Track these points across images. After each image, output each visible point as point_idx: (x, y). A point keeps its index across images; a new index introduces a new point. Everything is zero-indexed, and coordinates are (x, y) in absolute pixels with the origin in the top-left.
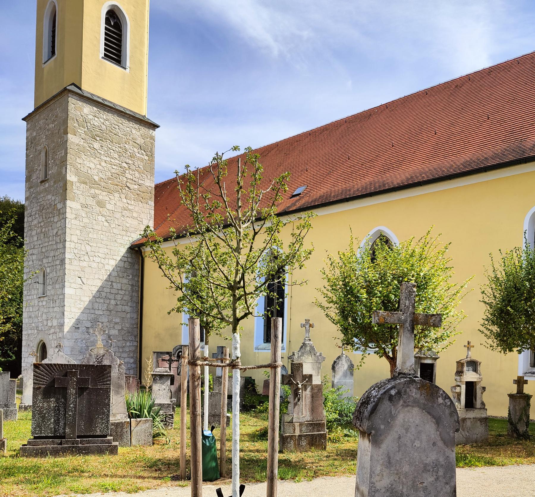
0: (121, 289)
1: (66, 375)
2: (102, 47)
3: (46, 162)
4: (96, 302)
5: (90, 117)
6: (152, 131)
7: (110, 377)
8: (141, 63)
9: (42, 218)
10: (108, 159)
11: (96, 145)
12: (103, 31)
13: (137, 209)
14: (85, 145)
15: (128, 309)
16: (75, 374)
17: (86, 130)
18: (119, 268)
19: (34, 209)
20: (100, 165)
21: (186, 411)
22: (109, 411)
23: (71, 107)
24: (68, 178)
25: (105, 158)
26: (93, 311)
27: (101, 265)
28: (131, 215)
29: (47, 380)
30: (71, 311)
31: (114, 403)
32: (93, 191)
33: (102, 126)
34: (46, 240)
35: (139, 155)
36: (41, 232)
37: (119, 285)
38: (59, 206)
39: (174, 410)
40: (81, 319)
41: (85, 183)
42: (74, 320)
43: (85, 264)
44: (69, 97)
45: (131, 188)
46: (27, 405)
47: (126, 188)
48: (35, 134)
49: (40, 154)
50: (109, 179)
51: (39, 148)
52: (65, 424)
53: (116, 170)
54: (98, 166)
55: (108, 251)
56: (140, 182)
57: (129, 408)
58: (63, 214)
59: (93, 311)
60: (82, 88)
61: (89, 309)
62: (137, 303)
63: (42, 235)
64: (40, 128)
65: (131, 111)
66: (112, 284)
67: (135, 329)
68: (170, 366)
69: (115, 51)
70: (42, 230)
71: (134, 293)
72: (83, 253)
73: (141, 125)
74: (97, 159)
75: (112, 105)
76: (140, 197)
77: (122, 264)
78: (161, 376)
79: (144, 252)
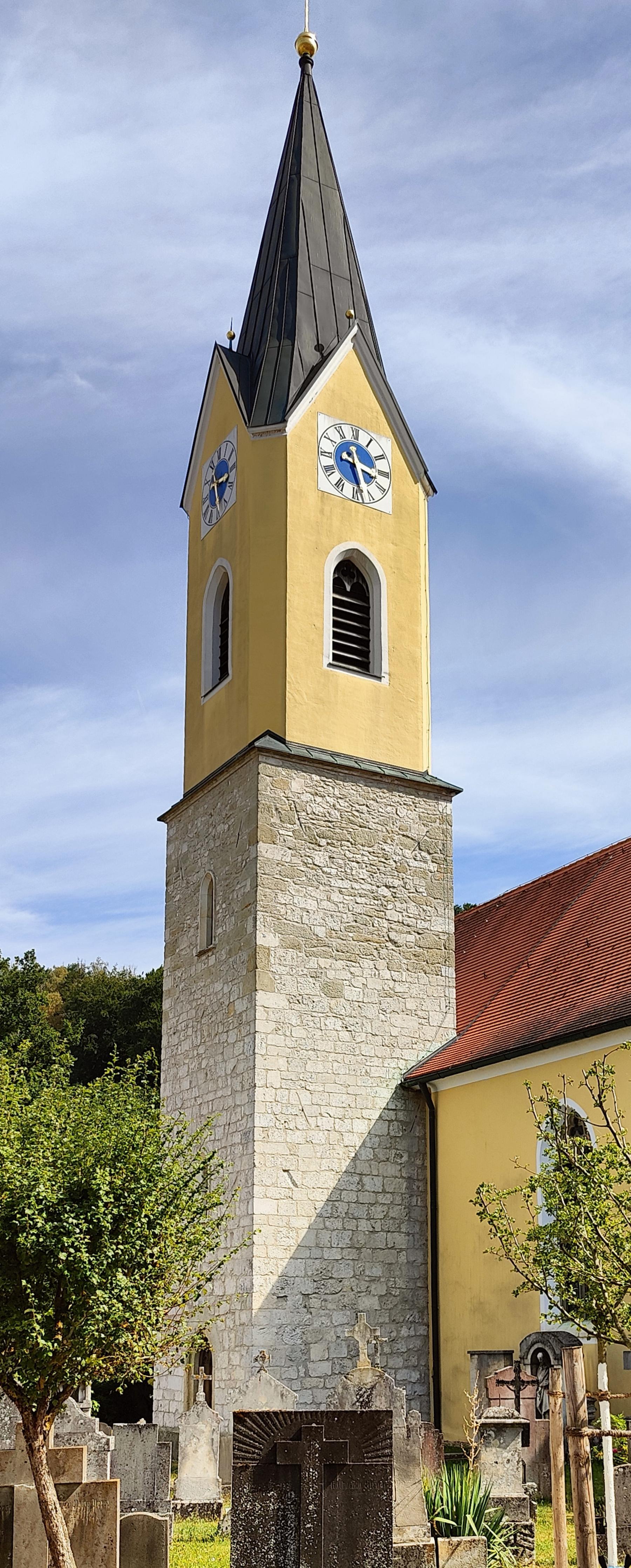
0: (384, 1192)
1: (298, 1437)
2: (328, 640)
3: (211, 909)
4: (326, 1228)
5: (306, 797)
6: (444, 804)
7: (391, 1438)
8: (415, 661)
9: (202, 1036)
10: (346, 884)
11: (320, 858)
12: (329, 607)
13: (414, 991)
14: (295, 860)
15: (400, 1240)
16: (315, 1434)
17: (296, 827)
18: (377, 1139)
19: (184, 1017)
20: (329, 899)
21: (565, 1515)
22: (390, 1520)
23: (264, 783)
24: (259, 941)
25: (340, 883)
26: (317, 1253)
27: (334, 1136)
28: (402, 1006)
29: (260, 1450)
30: (268, 1257)
31: (398, 1501)
32: (313, 963)
33: (333, 812)
34: (211, 1086)
35: (416, 864)
36: (200, 1068)
37: (378, 1181)
38: (240, 1006)
39: (533, 1515)
40: (291, 1274)
41: (297, 947)
42: (274, 1278)
43: (297, 1137)
44: (260, 763)
45: (400, 942)
46: (186, 1502)
47: (389, 944)
48: (185, 849)
49: (197, 890)
50: (348, 929)
51: (194, 878)
52: (298, 1551)
53: (364, 905)
54: (325, 904)
55: (350, 1100)
56: (421, 925)
57: (431, 1512)
58: (248, 1023)
59: (317, 1253)
60: (287, 739)
61: (309, 1249)
62: (422, 1223)
63: (201, 1076)
64: (197, 835)
65: (394, 768)
66: (361, 1180)
67: (420, 1292)
68: (518, 1398)
69: (356, 646)
70: (200, 1064)
71: (414, 1199)
72: (295, 1111)
73: (419, 796)
74: (321, 887)
75: (352, 764)
76: (421, 961)
77: (383, 1129)
78: (500, 1429)
79: (437, 1093)
